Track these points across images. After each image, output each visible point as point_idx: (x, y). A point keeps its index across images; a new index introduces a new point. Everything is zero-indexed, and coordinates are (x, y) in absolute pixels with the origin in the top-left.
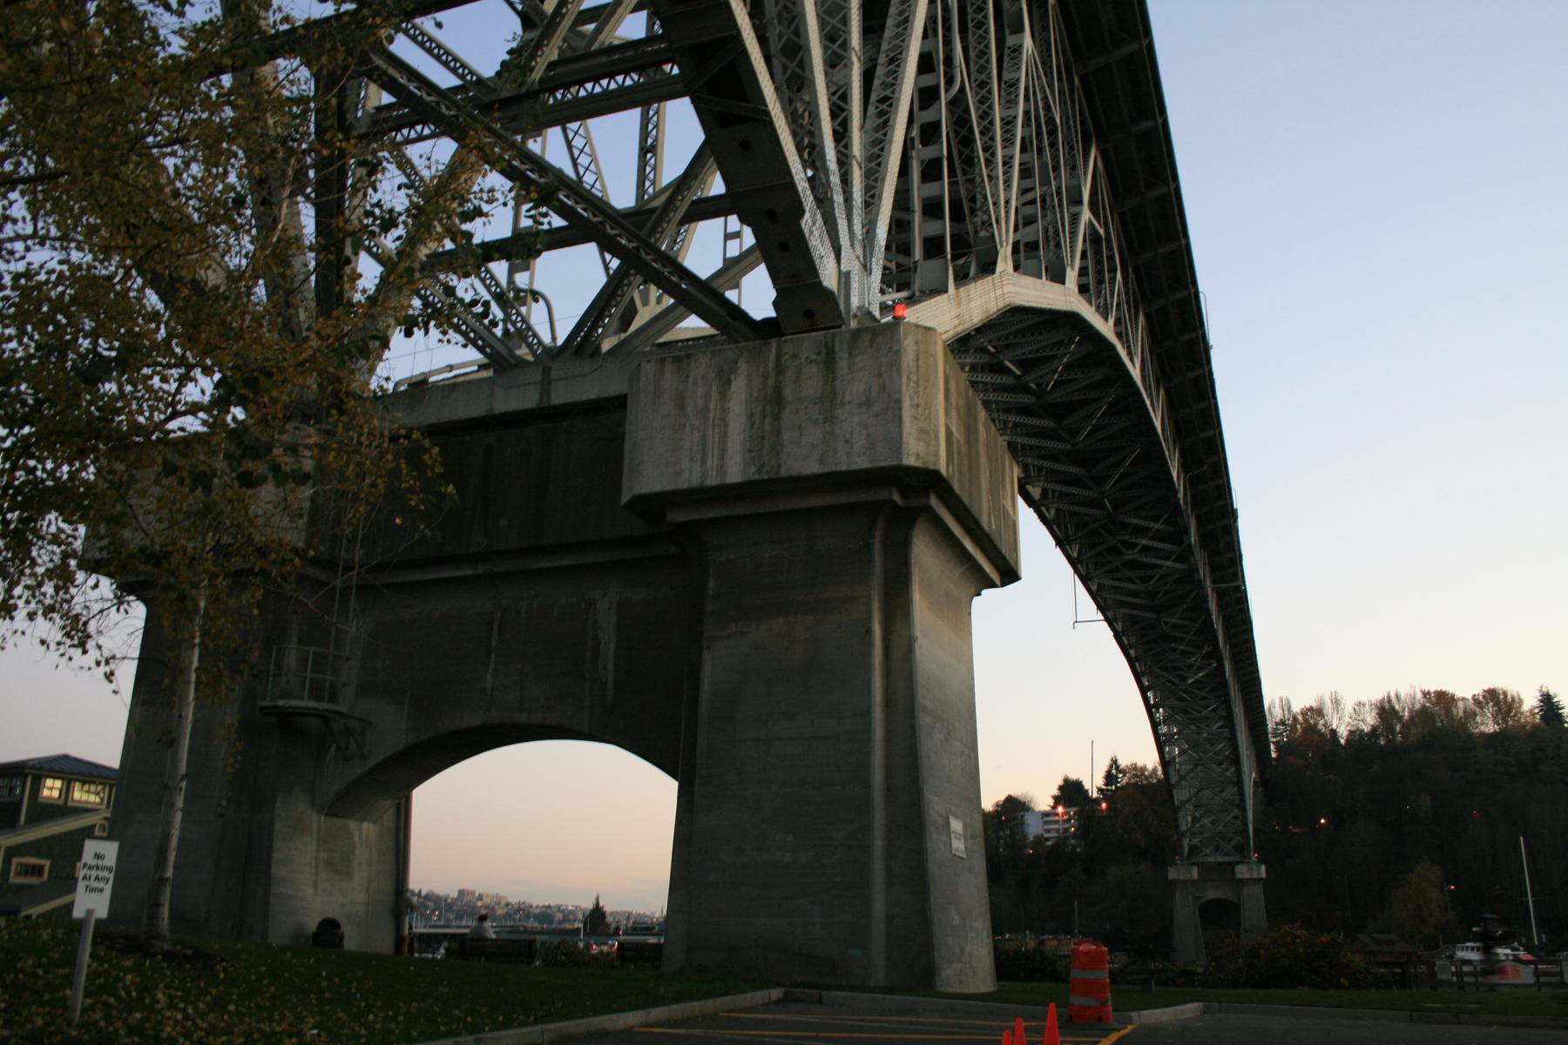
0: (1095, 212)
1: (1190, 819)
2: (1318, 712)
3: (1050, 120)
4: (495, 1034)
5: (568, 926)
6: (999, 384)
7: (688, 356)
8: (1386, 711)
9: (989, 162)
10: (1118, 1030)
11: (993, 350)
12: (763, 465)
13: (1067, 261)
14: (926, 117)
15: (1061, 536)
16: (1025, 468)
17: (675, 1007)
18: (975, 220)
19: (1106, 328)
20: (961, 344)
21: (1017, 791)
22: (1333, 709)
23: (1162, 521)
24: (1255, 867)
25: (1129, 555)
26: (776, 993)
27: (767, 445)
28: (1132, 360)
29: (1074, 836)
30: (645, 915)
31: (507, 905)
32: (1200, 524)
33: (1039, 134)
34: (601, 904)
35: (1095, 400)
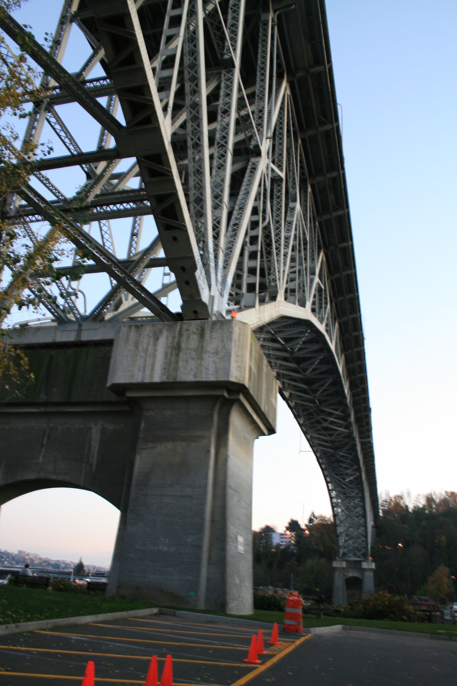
0: (320, 278)
2: (401, 497)
3: (305, 239)
4: (26, 623)
5: (66, 570)
6: (275, 347)
7: (142, 326)
9: (277, 254)
10: (304, 636)
11: (273, 333)
12: (169, 376)
13: (307, 298)
14: (253, 233)
15: (296, 414)
16: (283, 383)
17: (109, 614)
18: (270, 277)
19: (321, 328)
20: (260, 330)
21: (270, 524)
23: (339, 410)
24: (370, 563)
25: (325, 424)
26: (155, 610)
27: (172, 367)
28: (331, 342)
29: (294, 545)
30: (101, 568)
31: (40, 558)
32: (356, 413)
33: (300, 244)
34: (82, 561)
35: (314, 357)
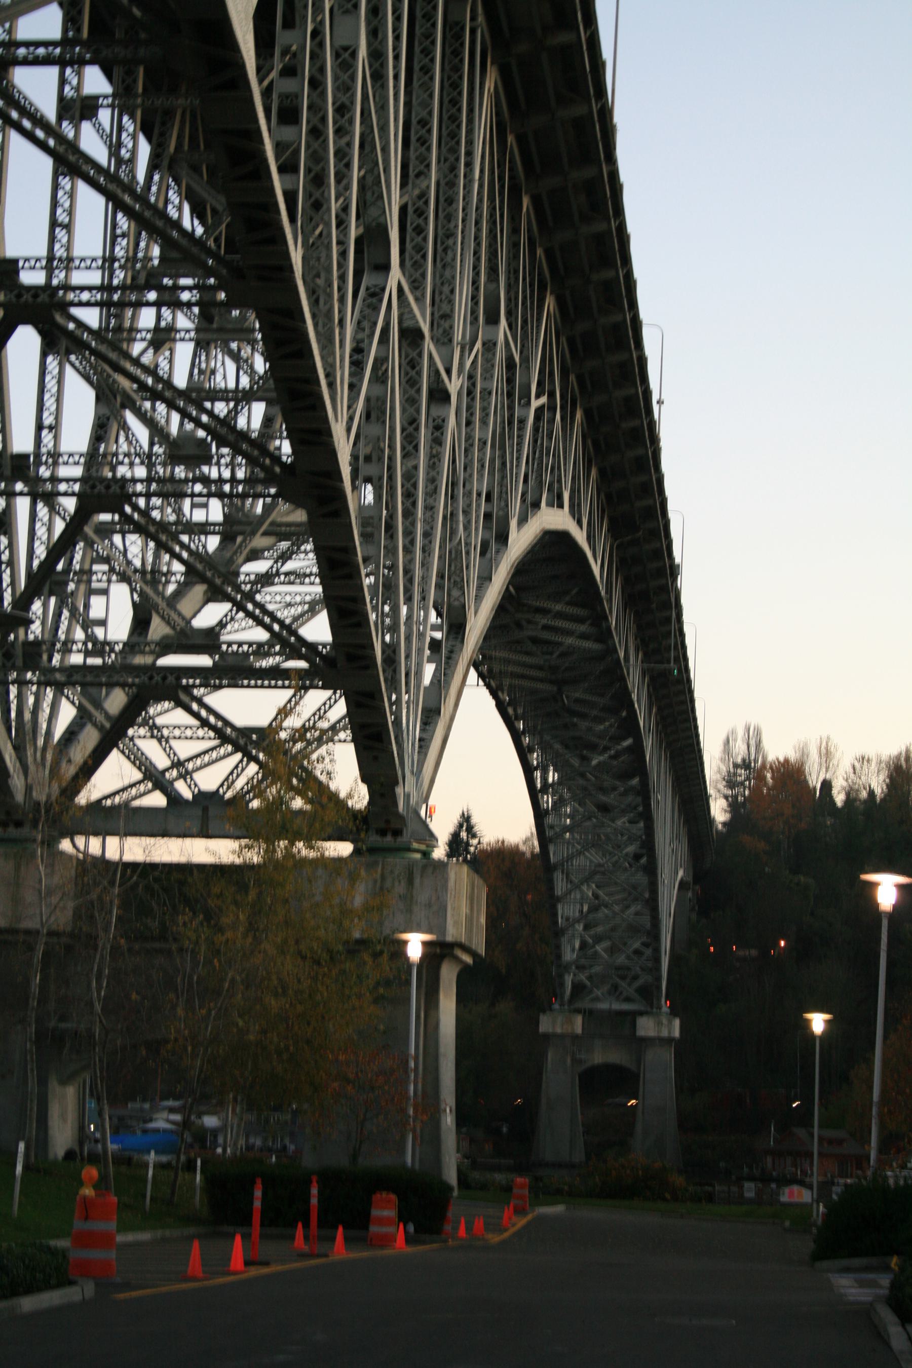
24: (665, 1021)
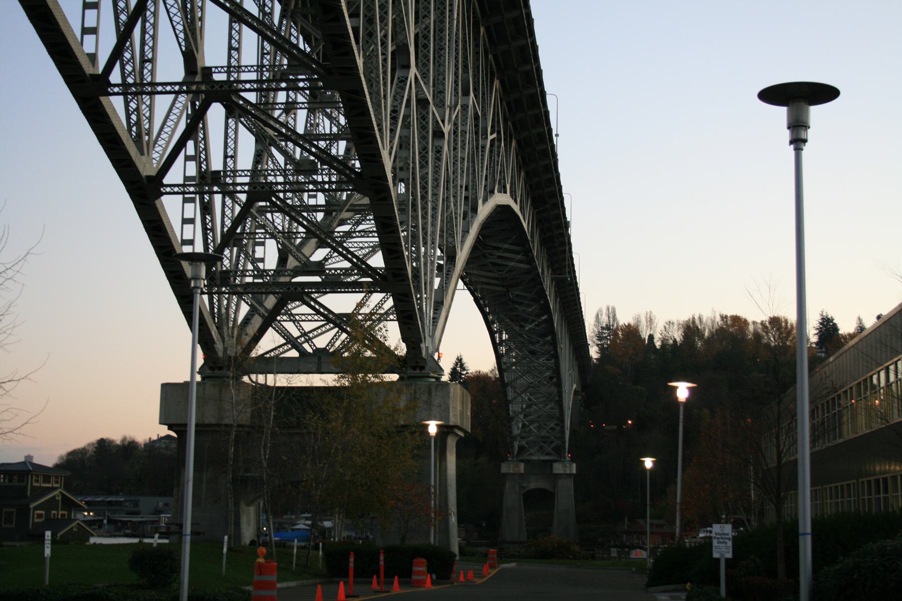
1: (520, 425)
8: (691, 330)
22: (647, 326)
